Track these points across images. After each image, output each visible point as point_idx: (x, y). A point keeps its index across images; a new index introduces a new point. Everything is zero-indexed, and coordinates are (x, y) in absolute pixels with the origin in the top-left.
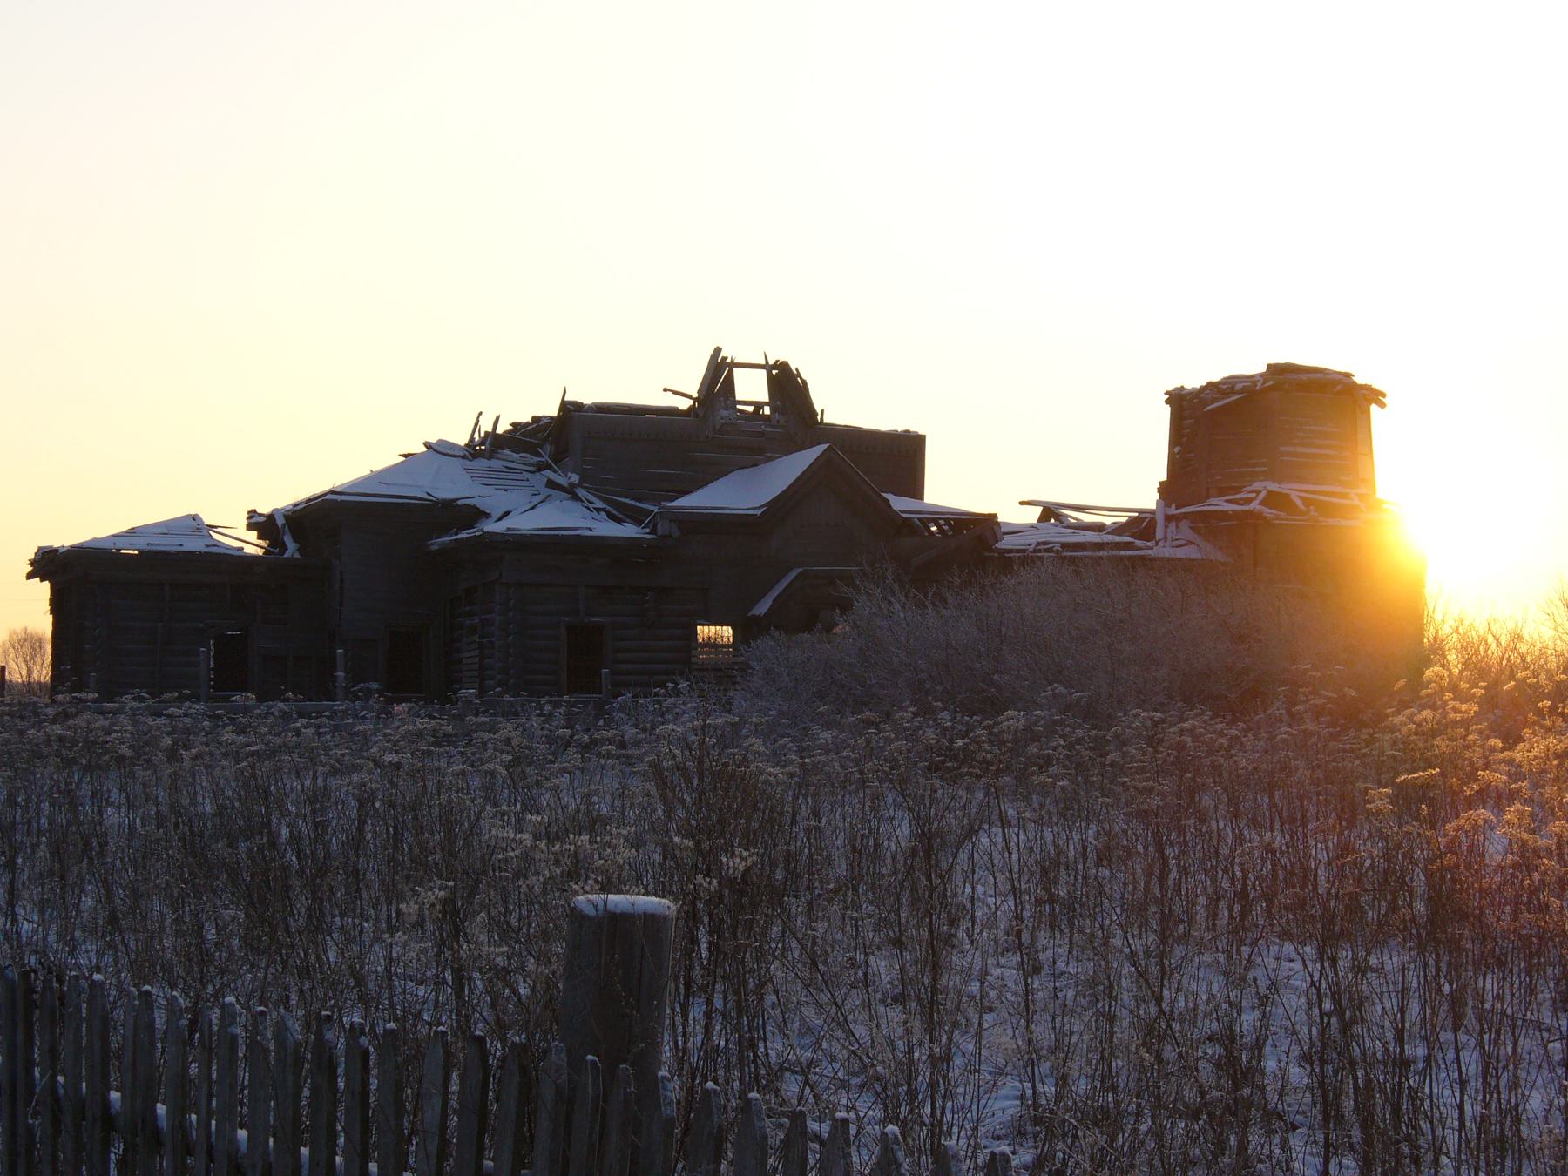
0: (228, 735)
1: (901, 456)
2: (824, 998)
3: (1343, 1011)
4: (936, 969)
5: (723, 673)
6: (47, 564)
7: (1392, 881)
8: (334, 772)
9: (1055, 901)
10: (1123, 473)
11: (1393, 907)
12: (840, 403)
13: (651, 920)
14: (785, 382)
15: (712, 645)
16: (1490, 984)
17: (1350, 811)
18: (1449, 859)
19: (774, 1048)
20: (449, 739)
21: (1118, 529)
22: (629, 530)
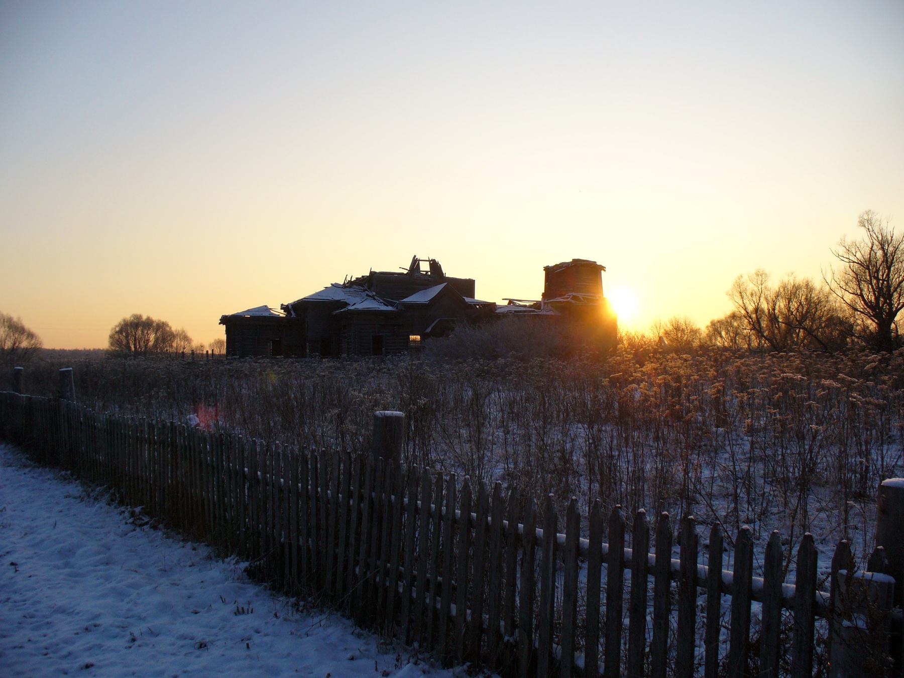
0: (276, 368)
1: (468, 286)
2: (447, 441)
3: (595, 442)
4: (480, 432)
5: (417, 349)
6: (225, 320)
7: (609, 406)
8: (306, 378)
9: (513, 412)
10: (530, 290)
11: (609, 413)
12: (449, 271)
13: (397, 418)
14: (434, 265)
15: (414, 341)
16: (636, 434)
17: (597, 386)
18: (625, 399)
19: (433, 456)
20: (339, 368)
21: (530, 306)
22: (390, 308)
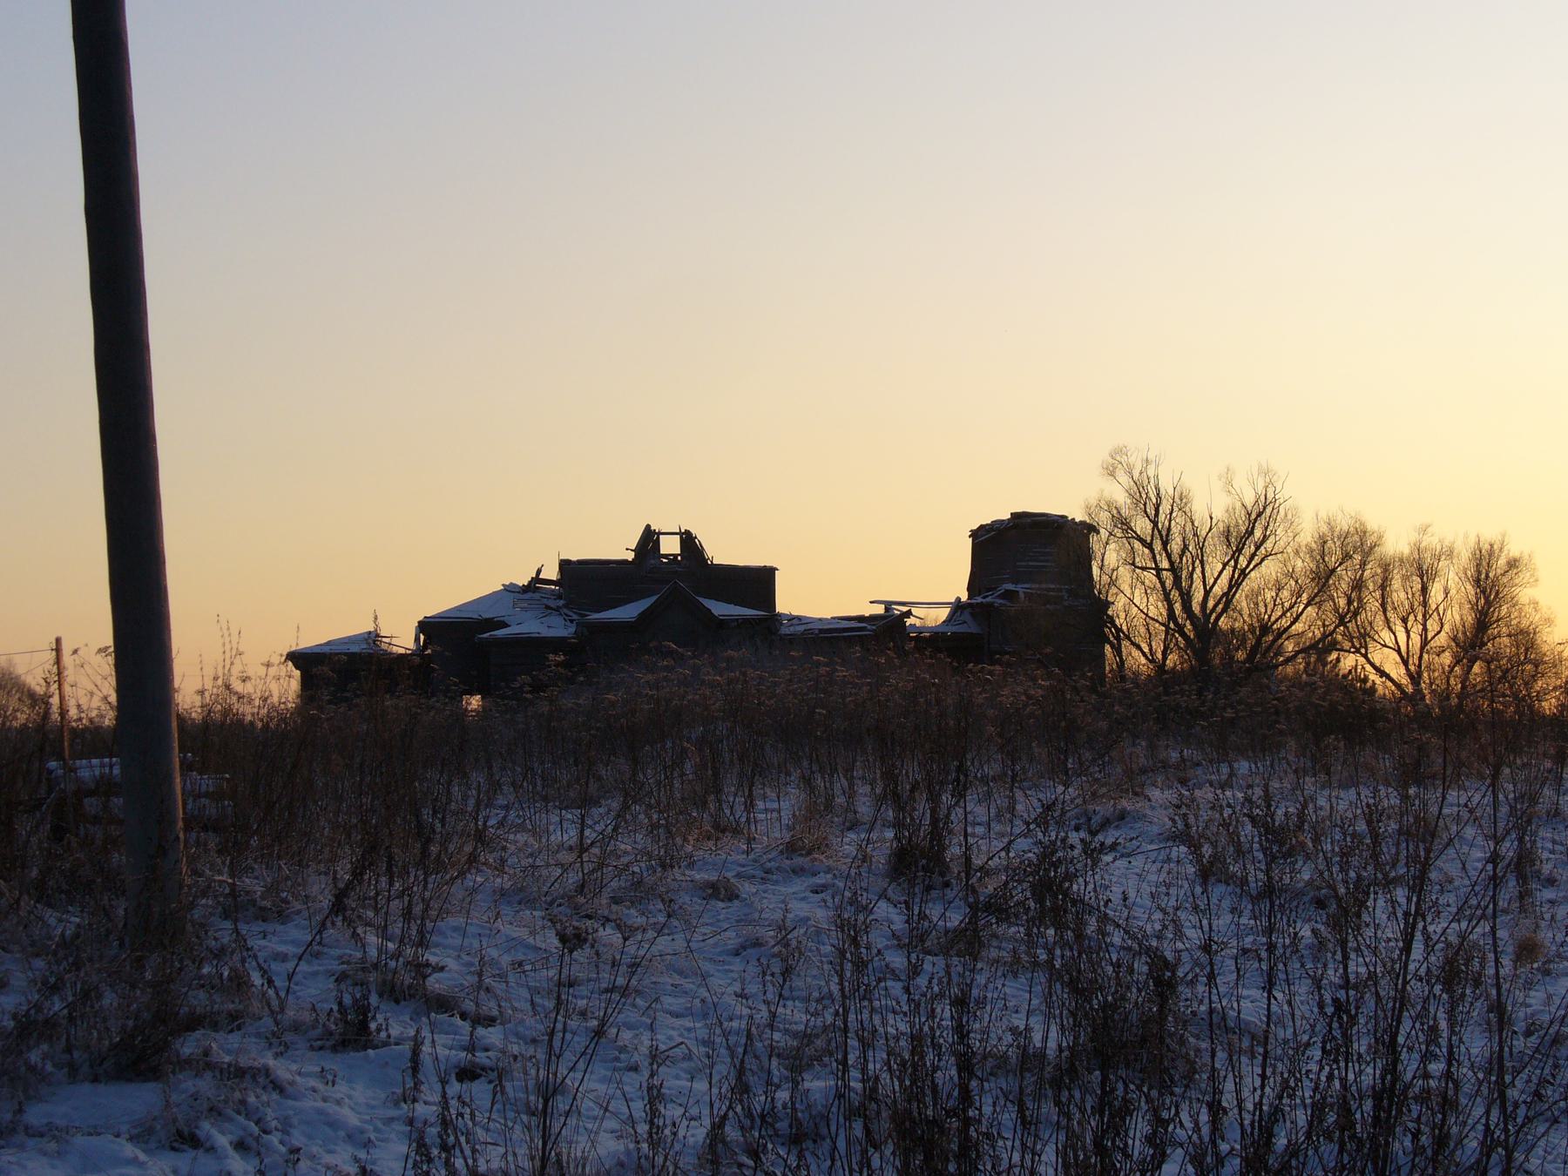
1: (758, 583)
10: (935, 582)
14: (688, 539)
